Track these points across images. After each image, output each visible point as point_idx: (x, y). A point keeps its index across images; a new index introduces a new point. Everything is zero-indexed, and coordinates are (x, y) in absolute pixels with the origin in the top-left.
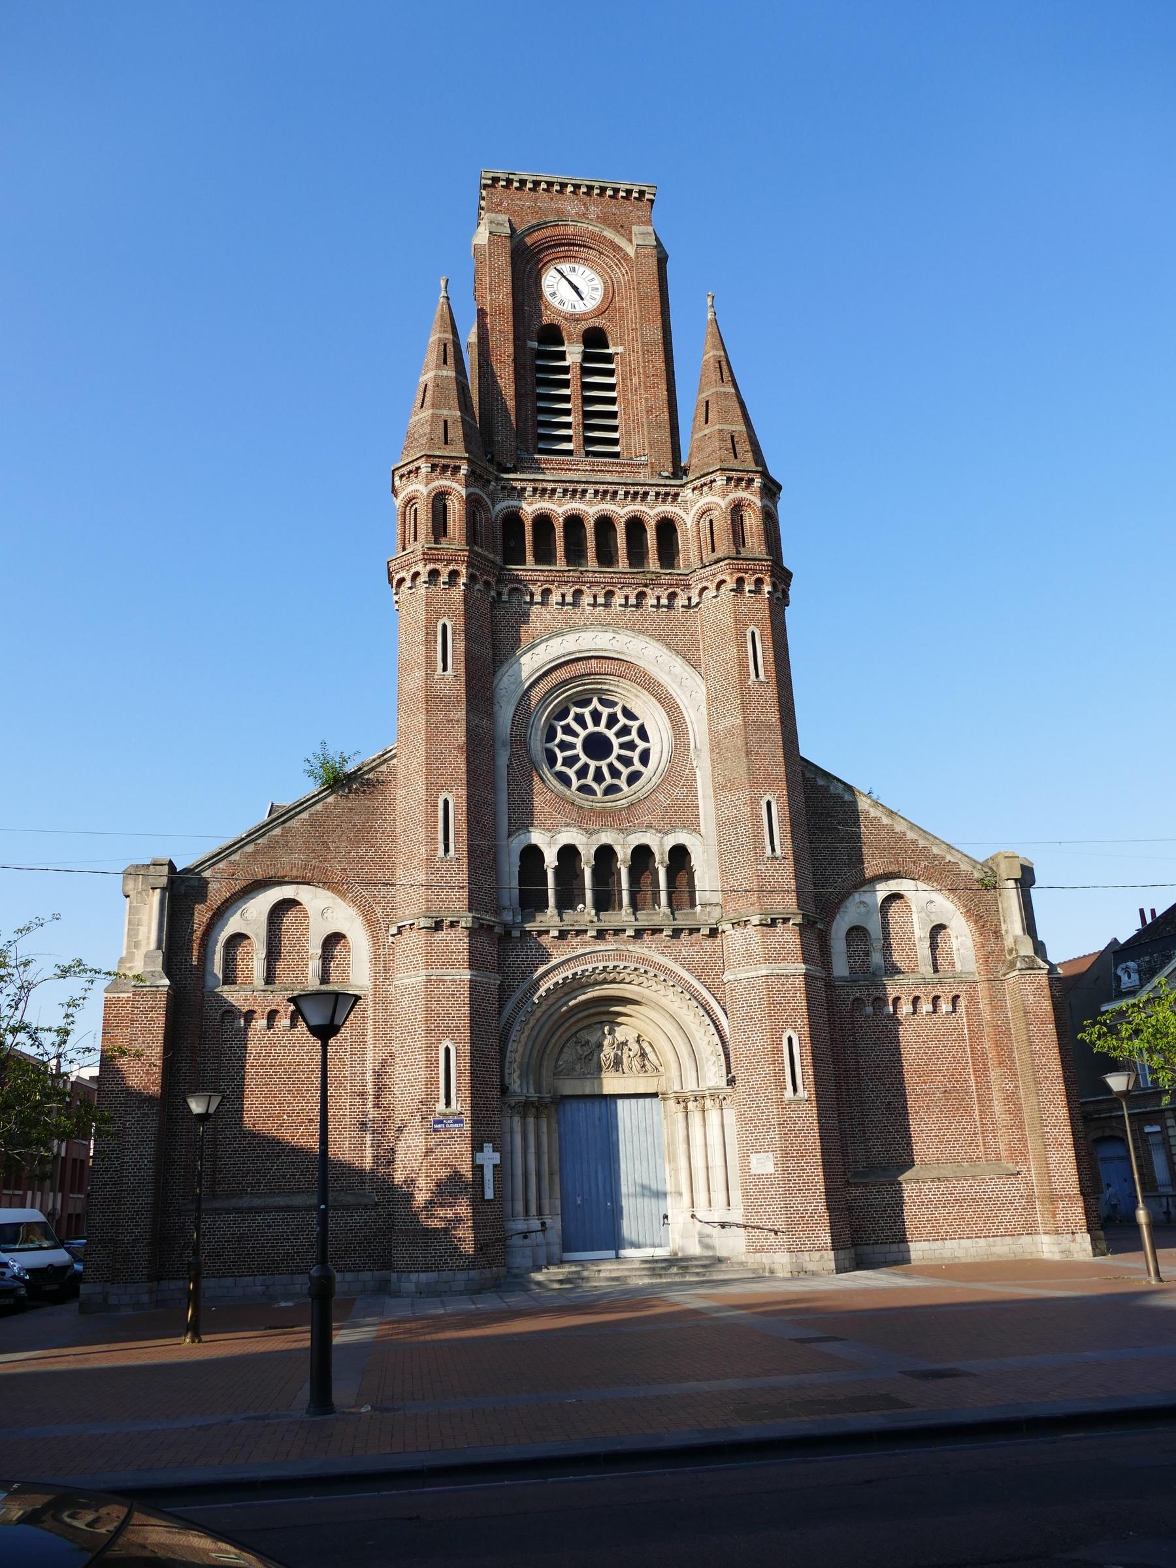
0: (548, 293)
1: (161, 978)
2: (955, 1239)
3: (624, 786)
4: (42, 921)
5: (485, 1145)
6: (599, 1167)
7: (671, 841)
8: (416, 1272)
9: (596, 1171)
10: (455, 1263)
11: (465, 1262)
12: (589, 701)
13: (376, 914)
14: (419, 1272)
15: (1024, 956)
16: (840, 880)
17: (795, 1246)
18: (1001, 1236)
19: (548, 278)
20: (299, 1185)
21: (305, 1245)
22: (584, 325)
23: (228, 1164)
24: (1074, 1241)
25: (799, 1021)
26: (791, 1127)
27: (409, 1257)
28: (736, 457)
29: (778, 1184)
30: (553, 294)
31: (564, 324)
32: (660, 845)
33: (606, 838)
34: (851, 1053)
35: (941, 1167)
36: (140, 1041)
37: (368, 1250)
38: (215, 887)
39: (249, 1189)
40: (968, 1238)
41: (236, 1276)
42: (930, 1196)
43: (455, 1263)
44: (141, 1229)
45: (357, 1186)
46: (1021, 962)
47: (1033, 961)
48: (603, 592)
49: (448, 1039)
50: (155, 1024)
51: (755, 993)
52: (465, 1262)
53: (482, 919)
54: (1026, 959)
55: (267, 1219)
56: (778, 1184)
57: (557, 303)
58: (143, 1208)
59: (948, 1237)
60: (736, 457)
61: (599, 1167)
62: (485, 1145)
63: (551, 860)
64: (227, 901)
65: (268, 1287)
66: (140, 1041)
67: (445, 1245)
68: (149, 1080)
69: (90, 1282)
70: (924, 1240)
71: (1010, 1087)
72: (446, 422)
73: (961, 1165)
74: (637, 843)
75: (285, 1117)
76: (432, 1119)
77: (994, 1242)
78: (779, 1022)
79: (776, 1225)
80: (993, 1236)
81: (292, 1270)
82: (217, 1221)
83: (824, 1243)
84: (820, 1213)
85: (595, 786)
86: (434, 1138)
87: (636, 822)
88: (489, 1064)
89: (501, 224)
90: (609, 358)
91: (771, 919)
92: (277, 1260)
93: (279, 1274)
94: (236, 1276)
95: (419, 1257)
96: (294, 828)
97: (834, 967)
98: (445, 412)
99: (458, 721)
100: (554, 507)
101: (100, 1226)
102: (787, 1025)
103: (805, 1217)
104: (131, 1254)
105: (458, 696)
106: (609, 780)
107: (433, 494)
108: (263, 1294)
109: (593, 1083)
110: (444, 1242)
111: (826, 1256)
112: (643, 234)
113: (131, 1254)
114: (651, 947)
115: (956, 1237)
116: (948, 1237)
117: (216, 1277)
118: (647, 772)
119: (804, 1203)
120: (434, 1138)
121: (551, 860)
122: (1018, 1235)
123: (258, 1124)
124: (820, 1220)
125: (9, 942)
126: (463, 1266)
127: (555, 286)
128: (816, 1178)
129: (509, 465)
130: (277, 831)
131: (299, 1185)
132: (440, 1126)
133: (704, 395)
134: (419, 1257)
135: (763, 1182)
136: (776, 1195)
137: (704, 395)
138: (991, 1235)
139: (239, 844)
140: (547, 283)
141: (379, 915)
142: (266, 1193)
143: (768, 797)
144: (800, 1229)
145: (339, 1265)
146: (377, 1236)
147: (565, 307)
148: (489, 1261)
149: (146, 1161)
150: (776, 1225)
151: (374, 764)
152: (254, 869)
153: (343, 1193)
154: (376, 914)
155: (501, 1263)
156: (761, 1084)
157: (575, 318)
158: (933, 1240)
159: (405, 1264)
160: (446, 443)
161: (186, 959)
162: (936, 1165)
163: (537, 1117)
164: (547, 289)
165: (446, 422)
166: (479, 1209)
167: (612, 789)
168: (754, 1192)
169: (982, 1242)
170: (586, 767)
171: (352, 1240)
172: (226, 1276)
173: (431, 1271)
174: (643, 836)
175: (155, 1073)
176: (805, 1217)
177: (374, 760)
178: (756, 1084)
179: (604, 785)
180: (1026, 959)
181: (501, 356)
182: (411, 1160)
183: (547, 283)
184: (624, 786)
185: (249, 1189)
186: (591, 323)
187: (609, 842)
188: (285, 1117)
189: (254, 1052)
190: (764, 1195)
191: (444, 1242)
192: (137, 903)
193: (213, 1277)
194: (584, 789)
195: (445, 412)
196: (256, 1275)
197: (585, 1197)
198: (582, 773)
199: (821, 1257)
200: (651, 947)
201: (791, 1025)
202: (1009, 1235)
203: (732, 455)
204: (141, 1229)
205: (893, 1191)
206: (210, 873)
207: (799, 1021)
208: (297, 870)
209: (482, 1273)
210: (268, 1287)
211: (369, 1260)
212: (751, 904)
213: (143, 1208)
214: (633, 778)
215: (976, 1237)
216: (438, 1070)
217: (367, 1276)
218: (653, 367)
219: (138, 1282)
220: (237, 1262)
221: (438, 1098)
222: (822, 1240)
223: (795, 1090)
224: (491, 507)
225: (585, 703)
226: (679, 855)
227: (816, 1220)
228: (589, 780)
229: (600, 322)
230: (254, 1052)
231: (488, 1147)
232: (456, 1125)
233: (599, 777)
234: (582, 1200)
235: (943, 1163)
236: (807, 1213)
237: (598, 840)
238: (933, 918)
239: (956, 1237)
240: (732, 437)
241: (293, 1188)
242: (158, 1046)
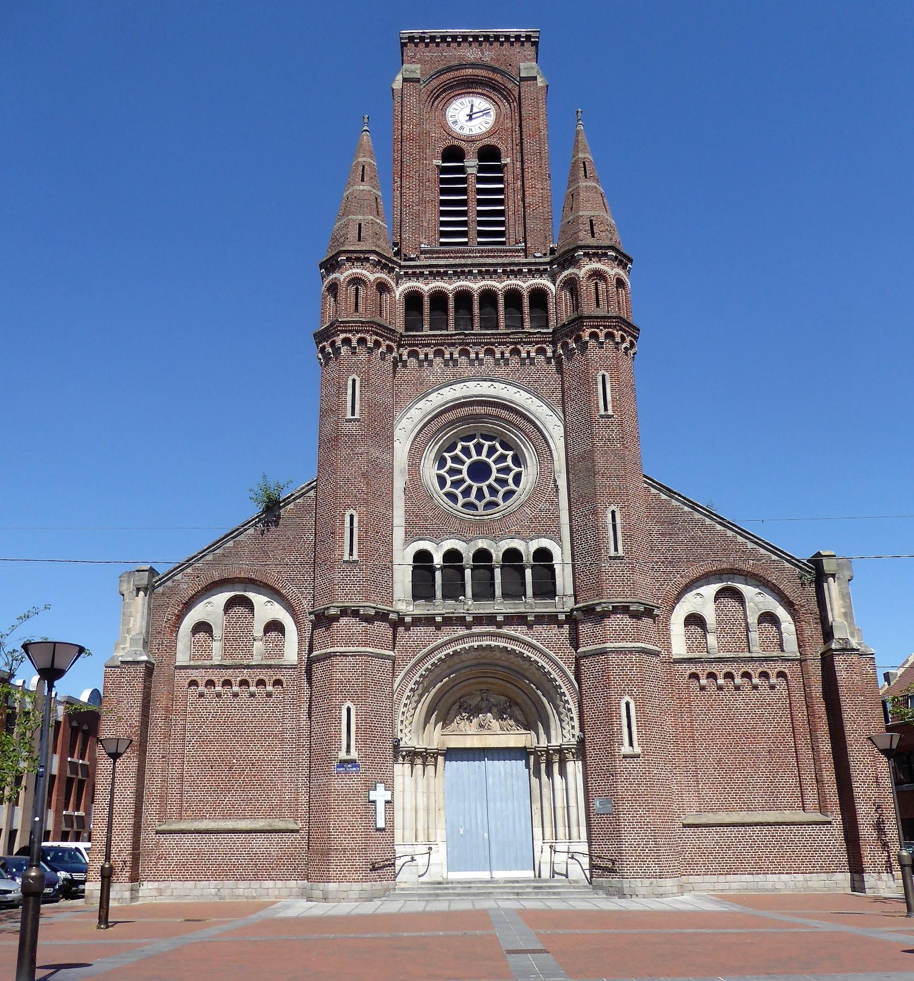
0: (451, 122)
1: (141, 655)
2: (775, 874)
3: (500, 501)
4: (37, 610)
5: (378, 784)
6: (478, 805)
7: (535, 545)
8: (323, 882)
9: (476, 808)
10: (352, 876)
11: (359, 876)
12: (510, 449)
13: (303, 606)
14: (324, 882)
15: (839, 638)
16: (679, 576)
17: (629, 874)
18: (816, 873)
19: (451, 110)
20: (244, 813)
21: (247, 859)
22: (479, 144)
23: (192, 796)
24: (880, 879)
25: (635, 689)
26: (626, 776)
27: (318, 871)
28: (593, 236)
29: (615, 822)
30: (455, 122)
31: (463, 145)
32: (528, 548)
33: (482, 544)
34: (687, 717)
35: (764, 814)
36: (125, 702)
37: (294, 864)
38: (184, 587)
39: (208, 815)
40: (787, 873)
41: (196, 880)
42: (754, 837)
43: (352, 876)
44: (125, 843)
45: (287, 815)
46: (835, 643)
47: (846, 643)
48: (483, 350)
49: (349, 701)
50: (136, 689)
51: (599, 667)
52: (359, 876)
53: (377, 608)
54: (840, 641)
55: (219, 838)
56: (615, 822)
57: (457, 129)
58: (126, 827)
59: (769, 872)
60: (593, 236)
61: (478, 805)
62: (378, 784)
63: (438, 560)
64: (193, 597)
65: (219, 890)
66: (125, 702)
67: (345, 862)
68: (131, 732)
69: (92, 881)
70: (748, 874)
71: (827, 748)
72: (360, 225)
73: (784, 813)
74: (506, 547)
75: (234, 761)
76: (336, 764)
77: (811, 877)
78: (618, 690)
79: (614, 856)
80: (809, 873)
81: (237, 878)
82: (183, 839)
83: (654, 872)
84: (650, 847)
85: (460, 496)
86: (337, 779)
87: (507, 531)
88: (660, 758)
89: (413, 72)
90: (499, 169)
91: (612, 606)
92: (226, 870)
93: (228, 880)
94: (196, 880)
95: (325, 871)
96: (242, 541)
97: (673, 647)
98: (360, 217)
99: (361, 454)
100: (445, 285)
101: (99, 840)
102: (624, 693)
103: (637, 850)
104: (118, 861)
105: (362, 435)
106: (488, 497)
107: (347, 280)
108: (216, 894)
109: (473, 739)
110: (343, 860)
111: (655, 883)
112: (527, 68)
113: (118, 861)
114: (517, 630)
115: (777, 872)
116: (769, 872)
117: (181, 881)
118: (519, 490)
119: (637, 839)
120: (337, 779)
121: (438, 560)
122: (832, 872)
123: (215, 766)
124: (651, 853)
125: (13, 626)
126: (358, 879)
127: (457, 116)
128: (648, 818)
129: (412, 256)
130: (230, 544)
131: (244, 813)
132: (342, 769)
133: (571, 189)
134: (325, 871)
135: (604, 820)
136: (614, 831)
137: (571, 189)
138: (807, 872)
139: (203, 554)
140: (450, 114)
141: (305, 606)
142: (220, 818)
143: (613, 507)
144: (634, 860)
145: (272, 875)
146: (301, 853)
147: (464, 132)
148: (380, 876)
149: (129, 792)
150: (614, 856)
151: (304, 491)
152: (213, 573)
153: (277, 820)
154: (303, 606)
155: (391, 878)
156: (602, 741)
157: (471, 140)
158: (756, 874)
159: (316, 876)
160: (359, 240)
161: (162, 642)
162: (761, 812)
163: (424, 765)
164: (450, 119)
165: (360, 225)
166: (372, 835)
167: (492, 504)
168: (597, 829)
169: (800, 877)
170: (470, 487)
171: (282, 856)
172: (189, 881)
173: (333, 882)
174: (512, 541)
175: (135, 726)
176: (637, 850)
177: (303, 488)
178: (599, 741)
179: (485, 501)
180: (840, 641)
181: (409, 172)
182: (321, 795)
183: (450, 114)
184: (500, 501)
185: (208, 815)
186: (486, 142)
187: (485, 546)
188: (234, 761)
189: (213, 711)
190: (605, 831)
191: (343, 860)
192: (129, 600)
193: (179, 881)
194: (468, 505)
195: (360, 217)
196: (210, 880)
197: (467, 829)
198: (466, 492)
199: (651, 883)
200: (517, 630)
201: (628, 693)
202: (824, 873)
203: (590, 235)
204: (125, 843)
205: (722, 832)
206: (181, 577)
207: (635, 689)
208: (245, 573)
209: (372, 885)
210: (219, 890)
211: (295, 872)
212: (597, 595)
213: (126, 827)
214: (508, 495)
215: (794, 873)
216: (340, 726)
217: (292, 884)
218: (532, 172)
219: (122, 882)
220: (197, 870)
221: (341, 747)
222: (652, 870)
223: (631, 744)
224: (395, 288)
225: (505, 446)
226: (543, 555)
227: (647, 853)
228: (472, 498)
229: (493, 141)
230: (213, 711)
231: (381, 787)
232: (354, 769)
233: (480, 495)
234: (464, 831)
235: (767, 810)
236: (639, 847)
237: (475, 545)
238: (760, 607)
239: (777, 872)
240: (591, 221)
241: (240, 816)
242: (138, 706)
